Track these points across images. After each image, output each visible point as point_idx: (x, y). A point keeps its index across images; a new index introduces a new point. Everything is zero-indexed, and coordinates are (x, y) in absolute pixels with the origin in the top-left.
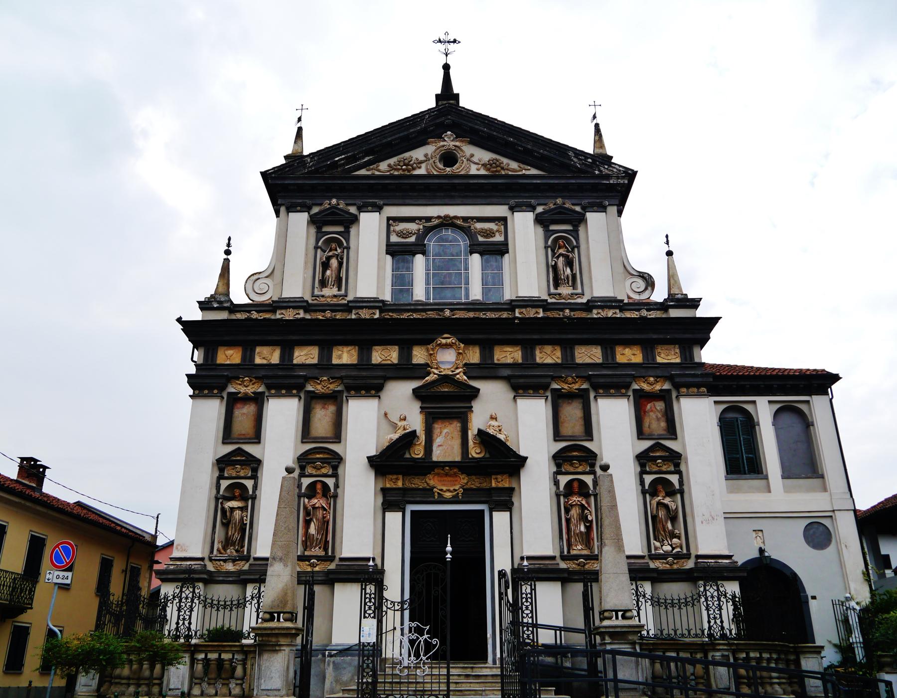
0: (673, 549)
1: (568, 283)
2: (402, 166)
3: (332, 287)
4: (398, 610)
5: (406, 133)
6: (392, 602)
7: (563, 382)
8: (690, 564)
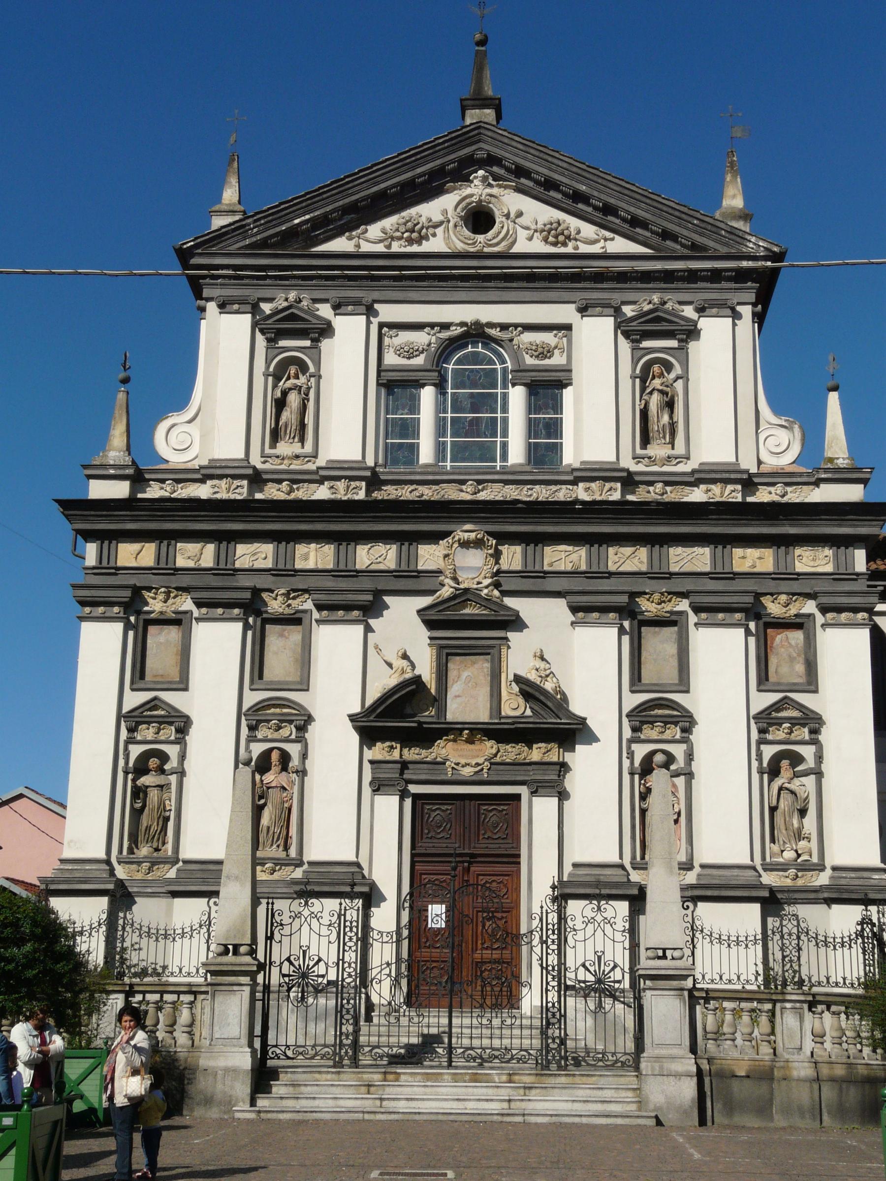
0: (799, 856)
1: (664, 437)
2: (403, 233)
3: (291, 441)
4: (387, 942)
5: (409, 175)
6: (380, 932)
7: (648, 600)
8: (823, 879)
